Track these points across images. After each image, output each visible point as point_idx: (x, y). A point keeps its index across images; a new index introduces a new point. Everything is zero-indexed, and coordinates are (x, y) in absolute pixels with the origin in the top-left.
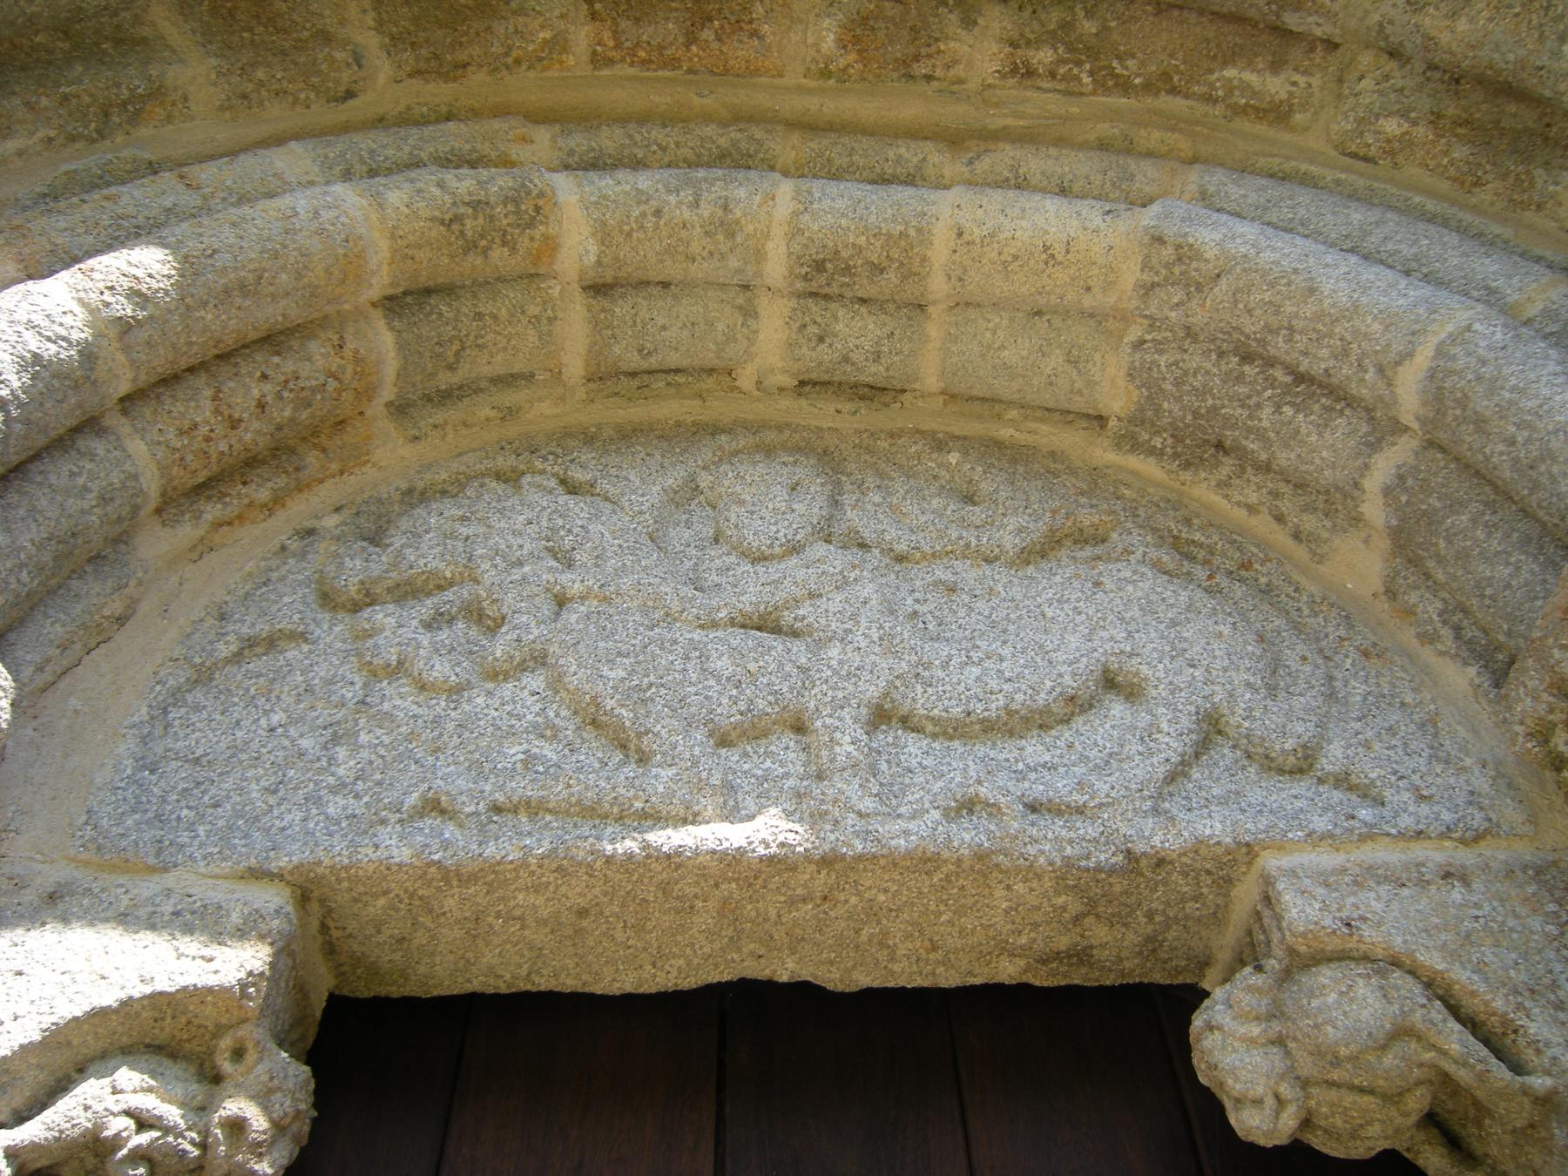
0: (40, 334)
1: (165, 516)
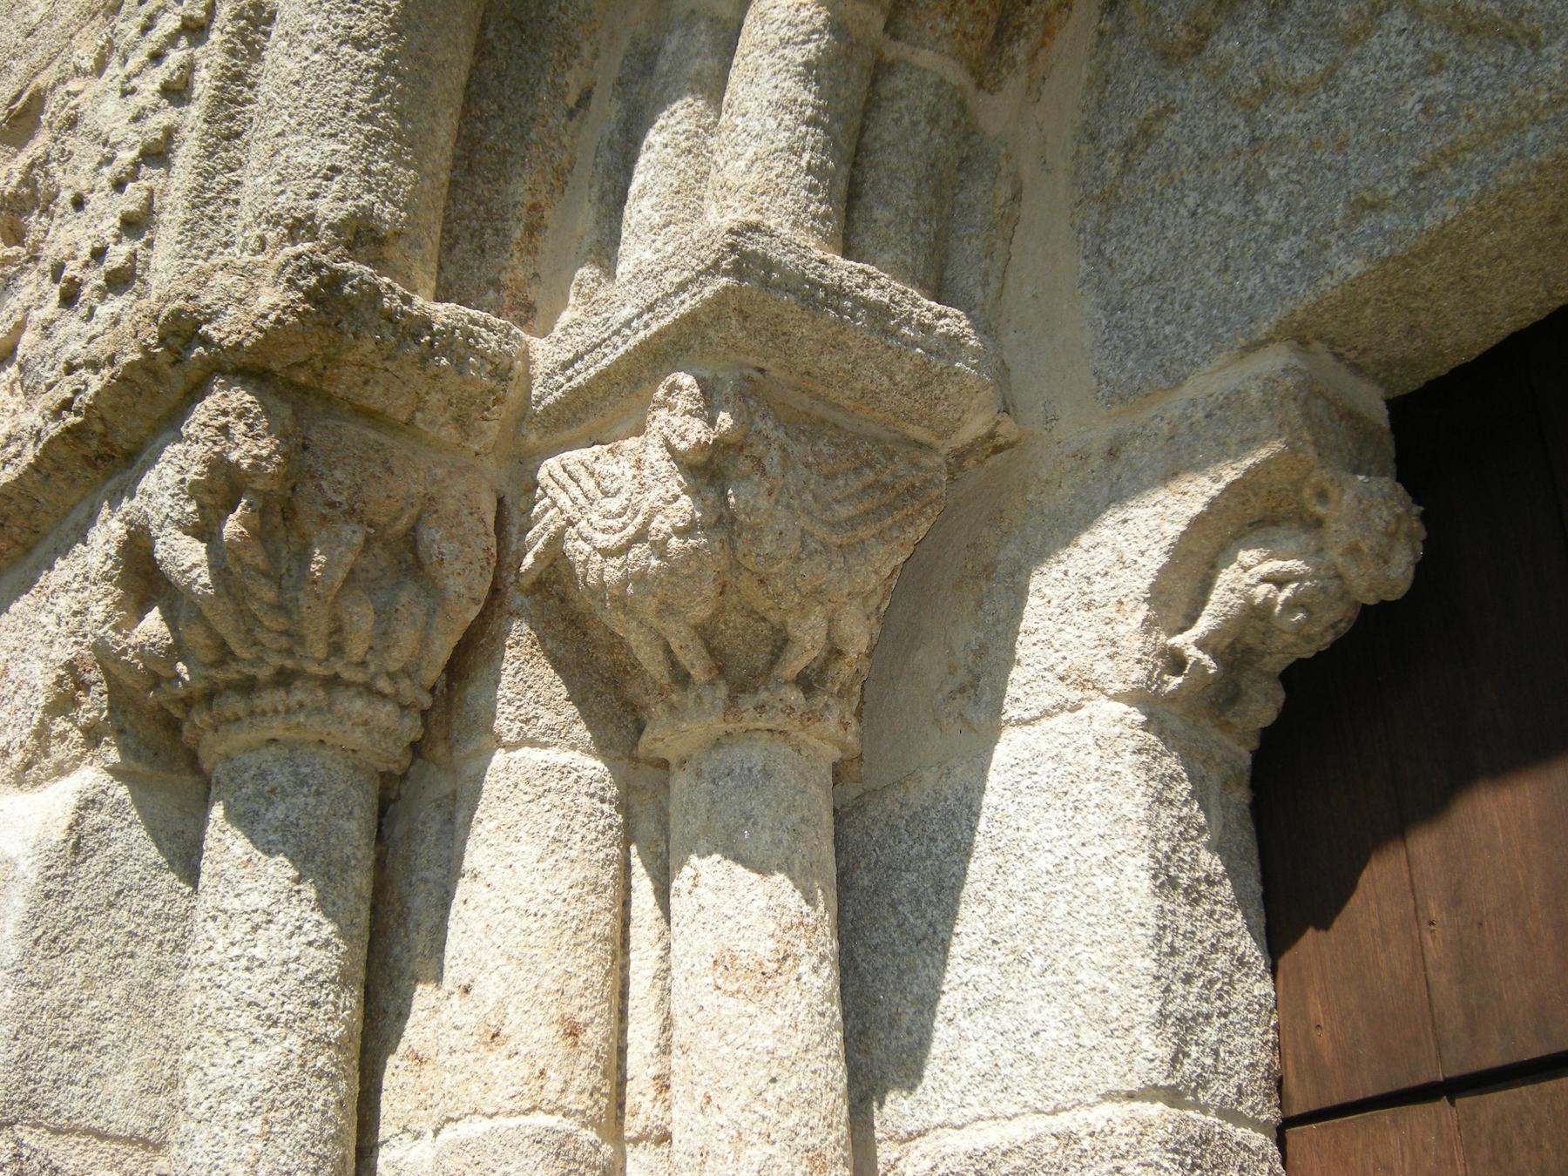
0: (796, 44)
1: (986, 84)
